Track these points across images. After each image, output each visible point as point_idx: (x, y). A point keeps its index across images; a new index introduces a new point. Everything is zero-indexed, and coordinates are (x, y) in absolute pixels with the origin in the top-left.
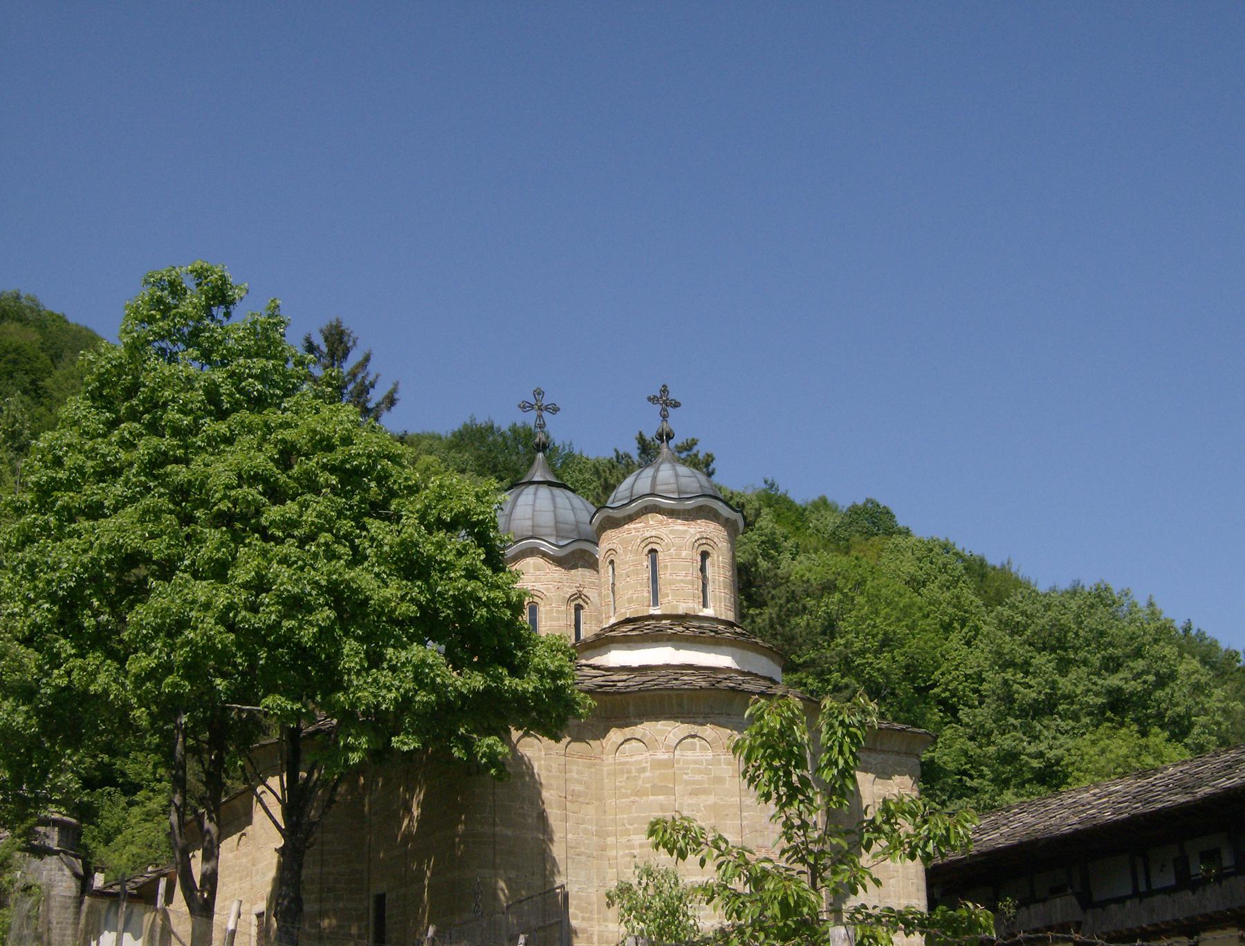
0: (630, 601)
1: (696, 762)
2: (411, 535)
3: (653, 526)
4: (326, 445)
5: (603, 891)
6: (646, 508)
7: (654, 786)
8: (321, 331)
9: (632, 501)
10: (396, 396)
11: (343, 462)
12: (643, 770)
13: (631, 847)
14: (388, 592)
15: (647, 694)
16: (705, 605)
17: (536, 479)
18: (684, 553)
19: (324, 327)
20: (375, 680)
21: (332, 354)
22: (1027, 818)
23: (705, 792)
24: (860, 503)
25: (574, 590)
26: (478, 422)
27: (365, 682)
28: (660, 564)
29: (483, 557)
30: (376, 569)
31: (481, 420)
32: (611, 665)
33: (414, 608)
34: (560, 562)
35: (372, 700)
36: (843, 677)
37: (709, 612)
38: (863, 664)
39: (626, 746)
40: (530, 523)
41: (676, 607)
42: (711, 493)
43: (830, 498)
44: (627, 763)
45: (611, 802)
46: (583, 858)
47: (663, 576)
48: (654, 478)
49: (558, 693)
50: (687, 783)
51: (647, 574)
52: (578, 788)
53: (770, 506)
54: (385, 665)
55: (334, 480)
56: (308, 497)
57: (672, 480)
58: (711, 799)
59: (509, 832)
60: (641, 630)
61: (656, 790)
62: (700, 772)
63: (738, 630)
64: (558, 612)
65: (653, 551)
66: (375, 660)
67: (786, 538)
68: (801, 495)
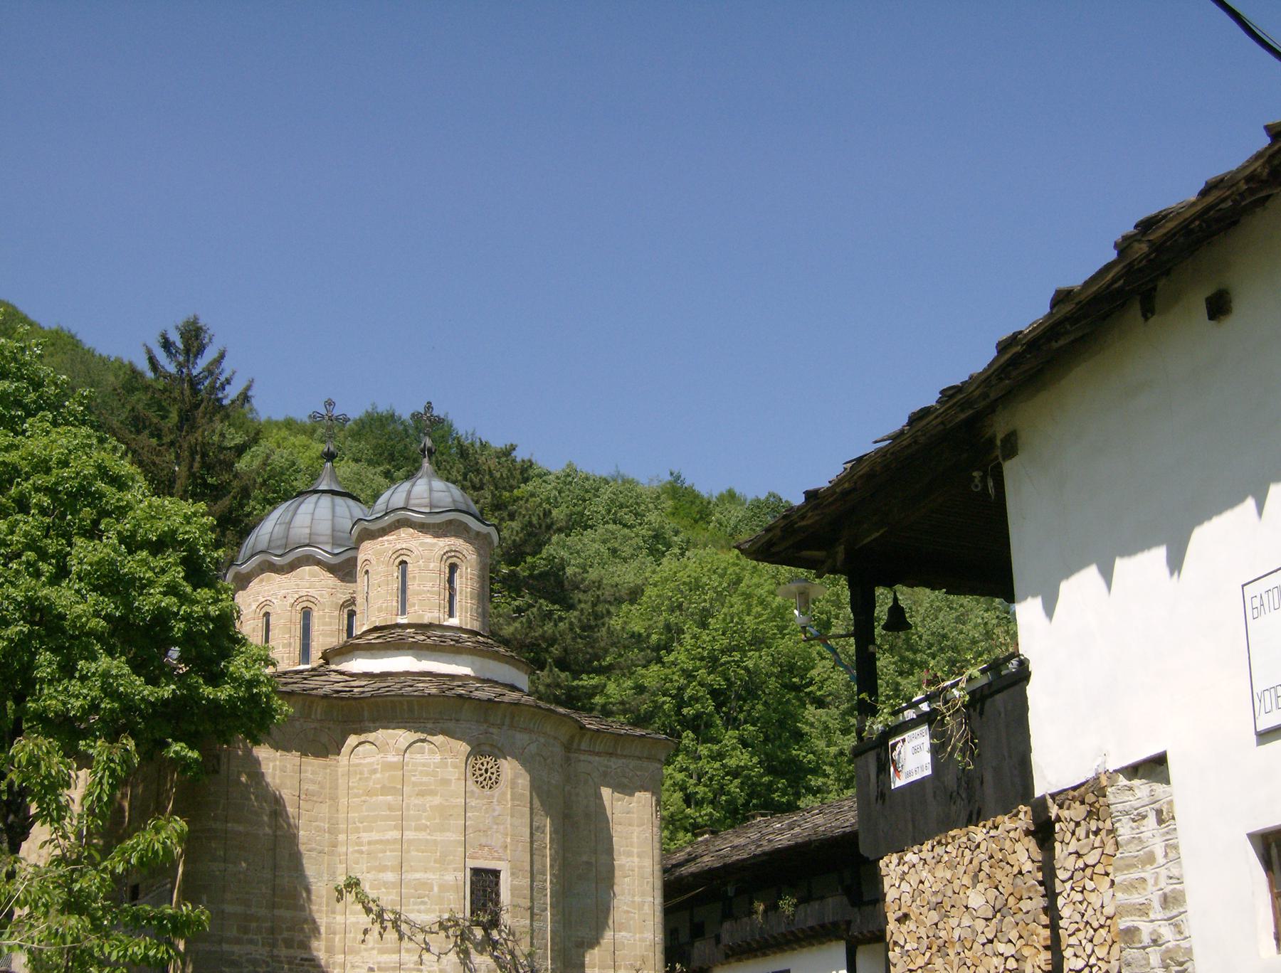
0: (380, 610)
1: (424, 765)
2: (109, 555)
3: (405, 539)
4: (43, 466)
5: (332, 885)
6: (398, 521)
7: (383, 787)
8: (177, 328)
9: (386, 514)
10: (250, 393)
11: (57, 484)
12: (374, 771)
13: (361, 844)
14: (75, 603)
15: (379, 700)
16: (451, 615)
17: (321, 488)
18: (432, 565)
19: (180, 324)
20: (66, 689)
21: (187, 351)
22: (820, 820)
23: (433, 793)
24: (763, 497)
25: (348, 597)
26: (379, 410)
27: (56, 690)
28: (409, 575)
29: (182, 574)
30: (76, 586)
31: (383, 408)
32: (355, 671)
33: (103, 623)
34: (332, 569)
35: (60, 706)
36: (709, 674)
37: (454, 622)
38: (728, 662)
39: (360, 748)
40: (307, 531)
41: (422, 616)
42: (464, 507)
43: (738, 491)
44: (359, 765)
45: (343, 801)
46: (314, 854)
47: (412, 586)
48: (409, 492)
49: (254, 699)
50: (414, 784)
51: (396, 585)
52: (312, 787)
53: (674, 498)
54: (77, 675)
55: (46, 501)
56: (19, 517)
57: (426, 495)
58: (437, 800)
59: (241, 828)
60: (389, 638)
61: (385, 790)
62: (427, 774)
63: (481, 639)
64: (331, 617)
65: (403, 563)
66: (67, 669)
67: (677, 533)
68: (708, 486)
